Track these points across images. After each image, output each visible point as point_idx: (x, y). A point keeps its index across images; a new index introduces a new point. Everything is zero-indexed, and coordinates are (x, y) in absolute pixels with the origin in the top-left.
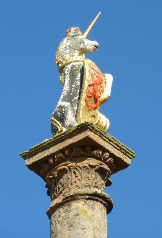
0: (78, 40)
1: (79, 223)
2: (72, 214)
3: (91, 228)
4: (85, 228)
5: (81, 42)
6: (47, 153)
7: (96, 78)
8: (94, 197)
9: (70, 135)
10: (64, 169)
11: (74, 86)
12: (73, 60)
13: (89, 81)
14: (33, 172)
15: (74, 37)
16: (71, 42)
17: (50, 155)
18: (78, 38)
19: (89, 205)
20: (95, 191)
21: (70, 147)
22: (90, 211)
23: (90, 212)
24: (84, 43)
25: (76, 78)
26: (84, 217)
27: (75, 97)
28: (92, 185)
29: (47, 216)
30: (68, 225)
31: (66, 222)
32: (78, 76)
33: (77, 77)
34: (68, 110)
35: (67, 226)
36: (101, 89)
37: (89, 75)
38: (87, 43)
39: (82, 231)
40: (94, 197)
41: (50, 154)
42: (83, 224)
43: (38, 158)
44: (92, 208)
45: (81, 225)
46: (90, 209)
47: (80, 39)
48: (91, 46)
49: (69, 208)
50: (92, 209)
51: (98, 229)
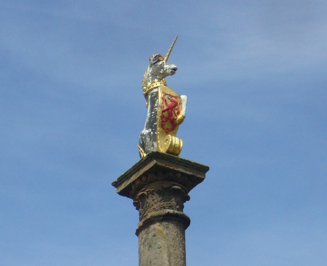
0: (158, 66)
2: (151, 235)
3: (166, 246)
4: (161, 247)
5: (162, 67)
6: (133, 178)
7: (169, 103)
8: (167, 218)
9: (143, 164)
11: (153, 113)
12: (153, 87)
13: (162, 107)
14: (126, 197)
16: (152, 69)
17: (132, 183)
18: (158, 64)
19: (164, 225)
20: (167, 212)
21: (146, 174)
22: (165, 230)
23: (165, 232)
24: (163, 68)
25: (154, 105)
26: (160, 237)
27: (155, 123)
28: (166, 206)
30: (148, 246)
31: (146, 243)
34: (147, 138)
35: (147, 247)
36: (176, 112)
37: (163, 102)
38: (167, 68)
39: (159, 250)
41: (132, 182)
42: (160, 243)
43: (124, 186)
44: (167, 228)
45: (157, 245)
46: (165, 229)
47: (160, 65)
48: (169, 70)
50: (167, 229)
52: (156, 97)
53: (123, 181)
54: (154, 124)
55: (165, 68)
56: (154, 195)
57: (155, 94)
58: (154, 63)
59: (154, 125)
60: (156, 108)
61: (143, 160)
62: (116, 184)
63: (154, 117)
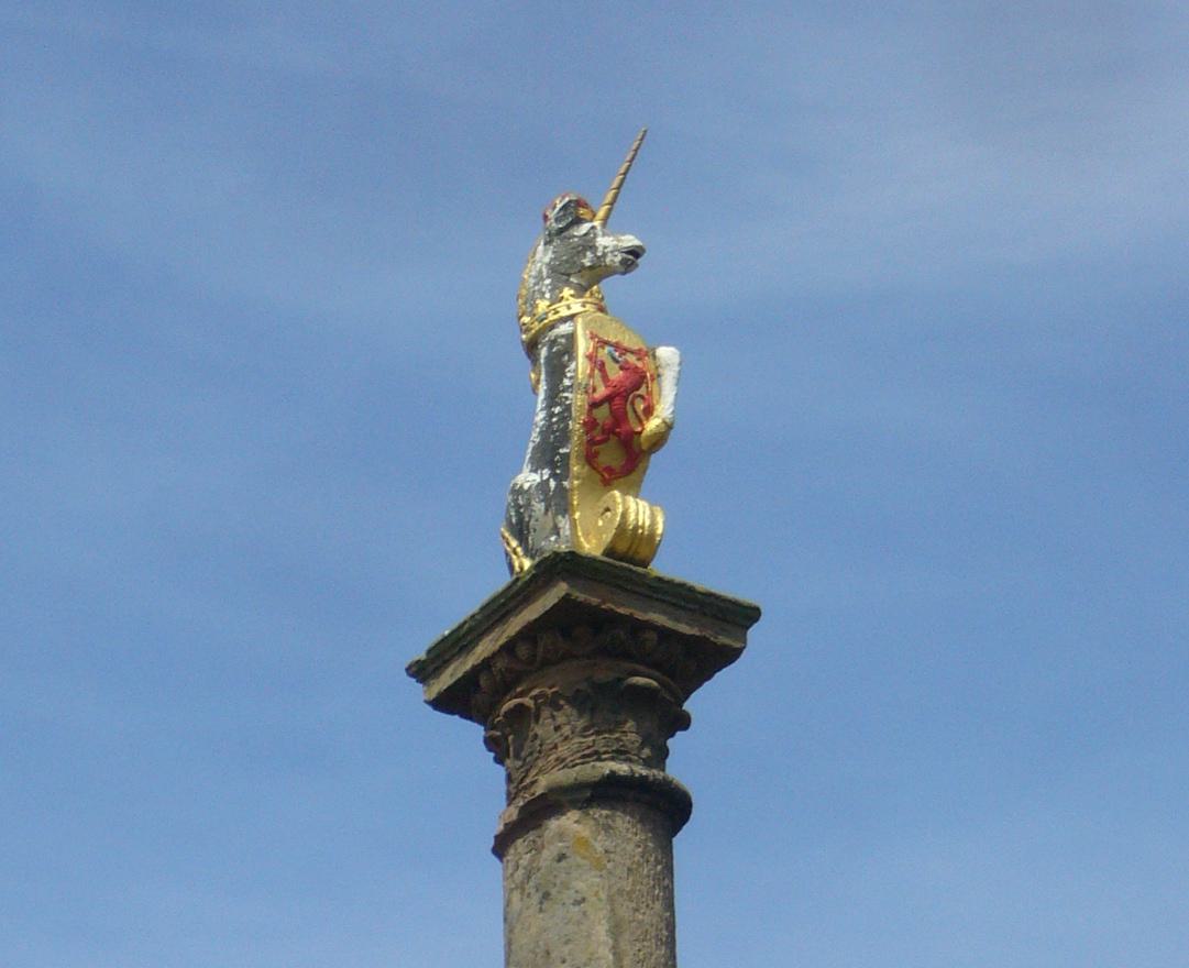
0: (576, 240)
1: (566, 886)
2: (548, 854)
3: (603, 896)
4: (584, 900)
5: (588, 244)
6: (485, 648)
7: (615, 373)
8: (607, 793)
10: (520, 708)
11: (557, 410)
13: (591, 391)
15: (564, 234)
16: (554, 252)
17: (479, 665)
18: (576, 234)
19: (595, 819)
20: (608, 772)
21: (529, 633)
22: (599, 838)
24: (593, 248)
27: (563, 447)
28: (605, 749)
29: (494, 859)
30: (540, 894)
32: (569, 375)
33: (566, 376)
34: (533, 503)
36: (641, 406)
37: (592, 370)
38: (605, 247)
39: (577, 909)
40: (607, 793)
41: (479, 661)
42: (580, 885)
43: (452, 675)
44: (607, 828)
49: (540, 837)
51: (628, 893)
52: (568, 352)
53: (447, 657)
54: (561, 451)
55: (601, 249)
56: (559, 708)
57: (563, 341)
58: (561, 231)
59: (562, 455)
60: (566, 394)
61: (519, 584)
62: (421, 671)
63: (562, 426)
